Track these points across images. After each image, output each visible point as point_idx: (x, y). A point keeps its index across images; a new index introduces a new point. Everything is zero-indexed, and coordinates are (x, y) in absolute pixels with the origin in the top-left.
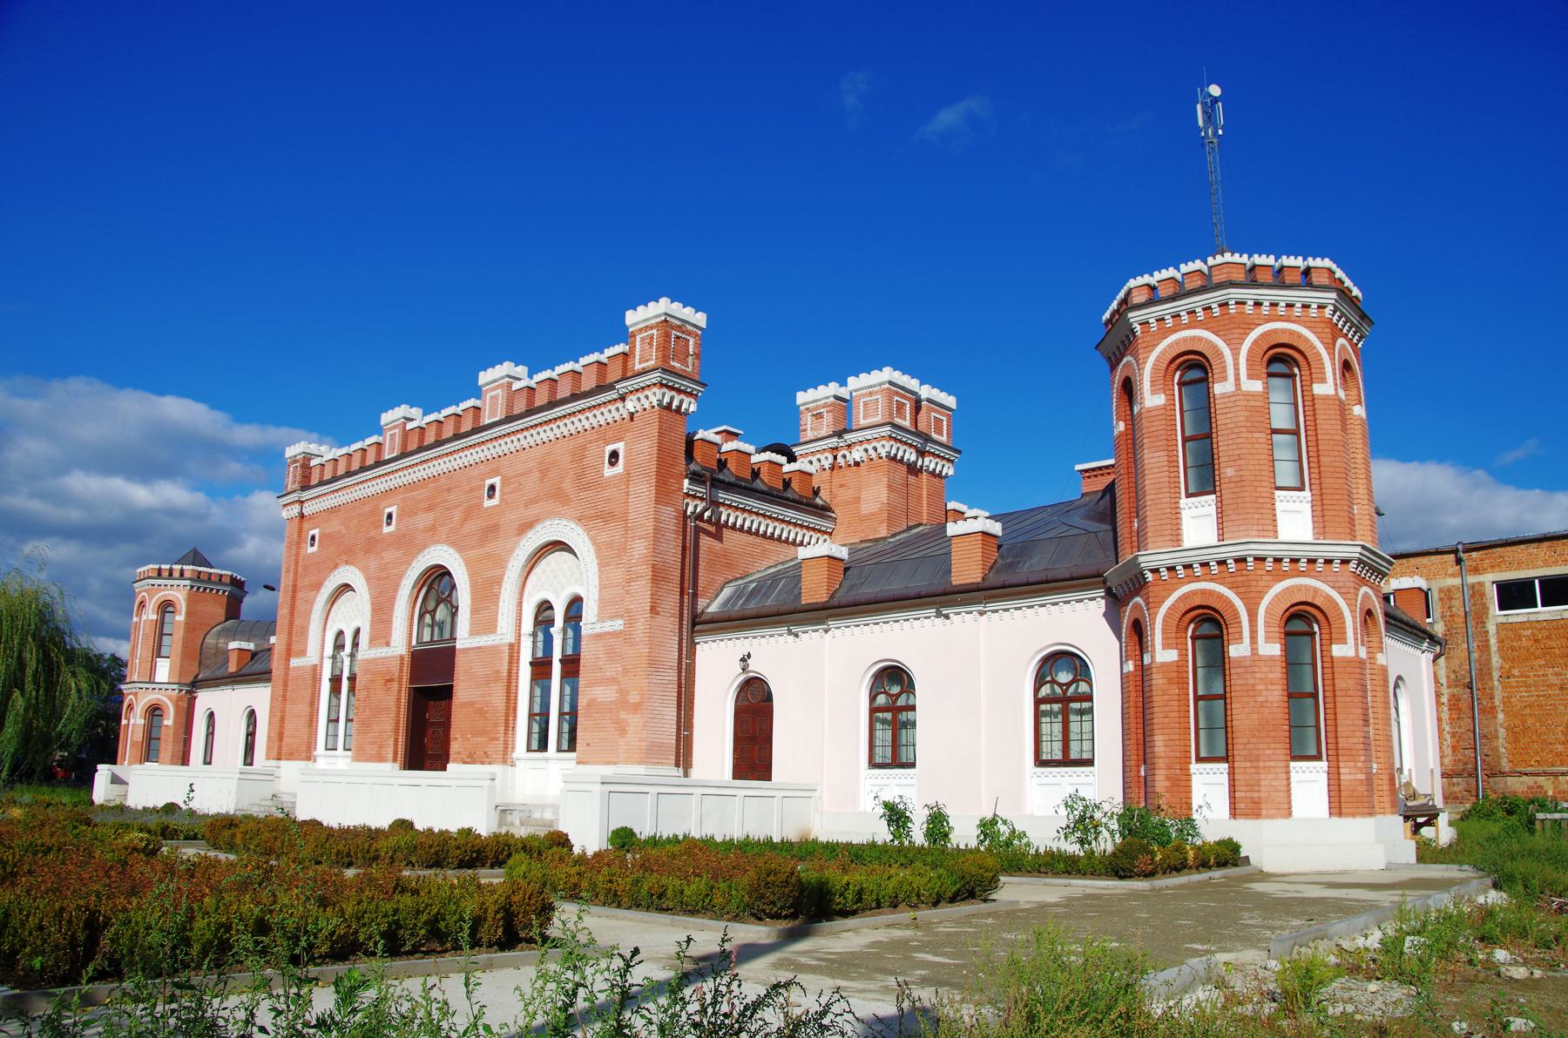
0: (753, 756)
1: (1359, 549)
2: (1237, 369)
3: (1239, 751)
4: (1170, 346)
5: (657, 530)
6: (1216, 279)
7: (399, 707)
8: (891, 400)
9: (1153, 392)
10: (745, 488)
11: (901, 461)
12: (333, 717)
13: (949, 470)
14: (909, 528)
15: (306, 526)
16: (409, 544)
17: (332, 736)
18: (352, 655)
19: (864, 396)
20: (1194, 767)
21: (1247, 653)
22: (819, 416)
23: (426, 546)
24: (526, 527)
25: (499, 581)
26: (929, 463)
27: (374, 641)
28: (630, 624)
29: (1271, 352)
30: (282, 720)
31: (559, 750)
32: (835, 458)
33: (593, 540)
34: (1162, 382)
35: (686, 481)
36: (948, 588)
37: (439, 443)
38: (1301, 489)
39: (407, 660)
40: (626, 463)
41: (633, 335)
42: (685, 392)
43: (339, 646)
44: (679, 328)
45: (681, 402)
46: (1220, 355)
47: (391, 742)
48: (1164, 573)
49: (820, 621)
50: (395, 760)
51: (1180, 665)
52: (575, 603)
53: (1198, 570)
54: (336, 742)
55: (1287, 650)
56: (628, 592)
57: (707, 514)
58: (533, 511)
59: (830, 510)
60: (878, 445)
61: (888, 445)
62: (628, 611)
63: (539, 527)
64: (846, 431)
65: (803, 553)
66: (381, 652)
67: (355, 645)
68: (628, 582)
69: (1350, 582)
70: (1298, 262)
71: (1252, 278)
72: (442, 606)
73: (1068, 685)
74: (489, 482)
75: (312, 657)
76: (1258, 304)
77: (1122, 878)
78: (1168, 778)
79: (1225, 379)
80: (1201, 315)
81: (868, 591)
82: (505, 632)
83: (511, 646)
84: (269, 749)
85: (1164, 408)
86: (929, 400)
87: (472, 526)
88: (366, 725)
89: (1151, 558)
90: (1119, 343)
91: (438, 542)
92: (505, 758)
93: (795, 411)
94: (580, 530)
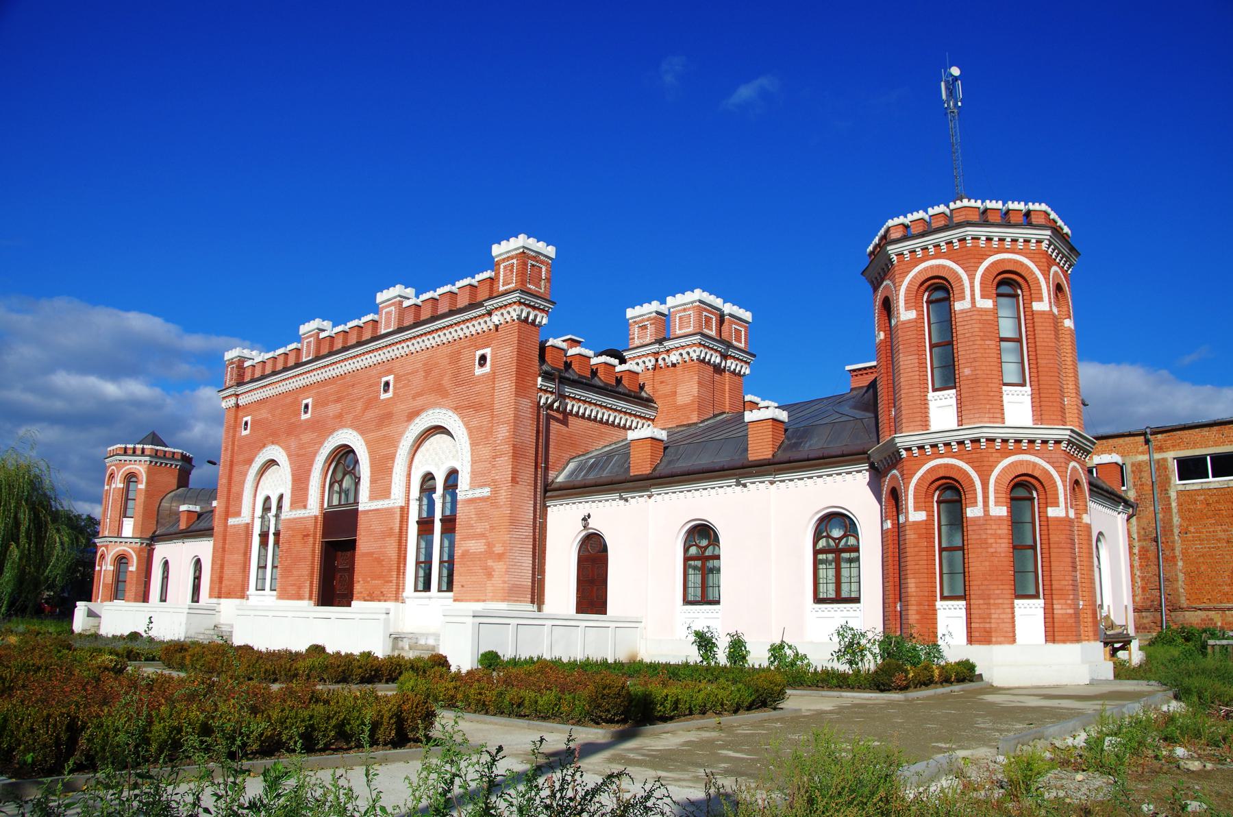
1: (1068, 432)
2: (972, 290)
3: (974, 591)
4: (920, 272)
5: (517, 417)
7: (313, 557)
8: (700, 315)
9: (907, 309)
11: (709, 363)
13: (746, 370)
15: (241, 414)
16: (322, 428)
18: (277, 516)
19: (679, 311)
21: (981, 514)
23: (334, 430)
24: (413, 415)
25: (392, 457)
26: (731, 364)
27: (294, 505)
28: (495, 491)
29: (1000, 277)
31: (440, 590)
32: (657, 360)
33: (466, 425)
35: (540, 379)
36: (746, 463)
38: (1023, 385)
39: (320, 519)
40: (492, 365)
41: (498, 264)
42: (538, 309)
43: (266, 509)
44: (534, 258)
45: (536, 316)
46: (959, 279)
48: (915, 451)
49: (645, 489)
50: (310, 598)
51: (928, 523)
52: (452, 475)
53: (942, 448)
54: (264, 584)
55: (1012, 511)
56: (494, 466)
57: (556, 405)
58: (419, 402)
59: (652, 401)
60: (691, 351)
61: (698, 350)
62: (494, 481)
63: (424, 415)
64: (665, 339)
65: (631, 435)
66: (300, 513)
67: (279, 507)
69: (1061, 458)
70: (1021, 206)
71: (984, 218)
72: (347, 477)
73: (840, 539)
74: (384, 379)
75: (245, 517)
76: (989, 239)
77: (882, 691)
78: (918, 612)
80: (944, 248)
81: (682, 465)
82: (397, 497)
83: (402, 508)
84: (211, 589)
85: (915, 321)
86: (730, 315)
87: (370, 414)
88: (287, 571)
89: (905, 439)
90: (880, 270)
92: (397, 597)
94: (456, 417)
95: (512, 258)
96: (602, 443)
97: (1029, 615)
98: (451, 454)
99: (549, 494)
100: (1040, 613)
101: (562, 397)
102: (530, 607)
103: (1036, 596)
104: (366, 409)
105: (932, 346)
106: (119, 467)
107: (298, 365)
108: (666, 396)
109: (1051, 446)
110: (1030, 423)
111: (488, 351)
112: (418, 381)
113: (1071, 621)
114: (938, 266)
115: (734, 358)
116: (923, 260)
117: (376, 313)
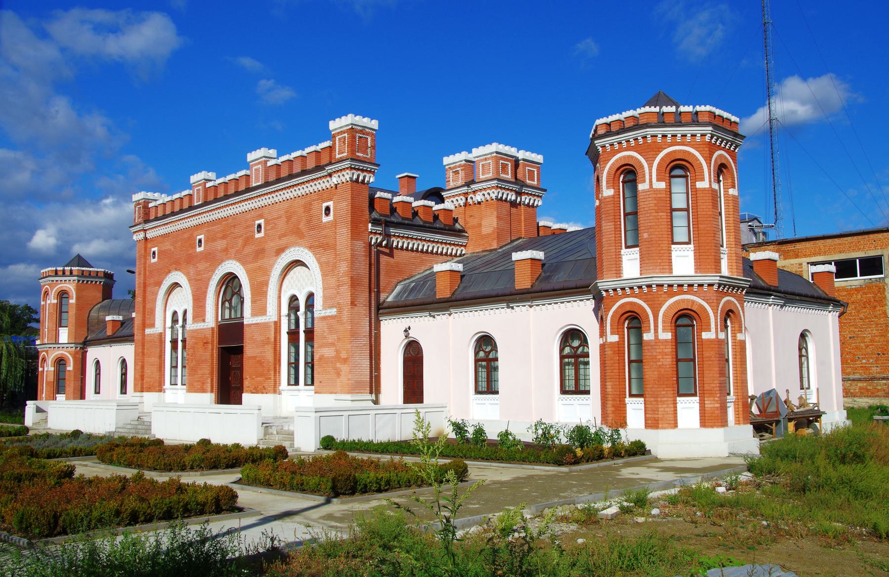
0: (413, 390)
1: (718, 278)
2: (651, 176)
3: (648, 392)
5: (353, 256)
6: (641, 122)
7: (212, 360)
8: (497, 163)
9: (608, 188)
10: (408, 225)
11: (506, 200)
12: (174, 365)
13: (540, 203)
14: (512, 241)
15: (149, 245)
16: (213, 260)
17: (174, 376)
18: (183, 327)
19: (482, 160)
20: (624, 251)
21: (653, 338)
22: (457, 172)
23: (222, 261)
24: (280, 251)
25: (266, 284)
26: (526, 199)
28: (340, 311)
29: (672, 164)
30: (143, 367)
31: (306, 384)
32: (467, 199)
33: (318, 260)
34: (613, 183)
35: (370, 225)
36: (513, 291)
37: (227, 197)
38: (689, 243)
40: (334, 215)
41: (334, 136)
42: (366, 171)
43: (175, 321)
44: (361, 132)
45: (364, 177)
46: (642, 167)
47: (209, 381)
48: (611, 292)
49: (446, 309)
50: (212, 391)
51: (620, 344)
52: (310, 296)
53: (628, 291)
54: (176, 380)
55: (676, 336)
57: (384, 243)
58: (284, 241)
59: (464, 231)
60: (491, 192)
61: (496, 192)
62: (339, 304)
63: (287, 251)
64: (473, 182)
65: (437, 268)
67: (185, 320)
68: (339, 286)
69: (713, 296)
70: (689, 109)
71: (662, 121)
72: (235, 296)
73: (578, 348)
74: (257, 222)
75: (158, 328)
76: (664, 136)
77: (559, 465)
78: (613, 406)
79: (644, 181)
80: (633, 143)
81: (473, 291)
83: (275, 323)
84: (135, 385)
85: (613, 197)
86: (524, 160)
87: (248, 250)
88: (193, 371)
90: (594, 156)
91: (228, 258)
92: (275, 390)
93: (443, 169)
95: (344, 132)
96: (423, 268)
97: (688, 409)
98: (308, 281)
99: (381, 311)
100: (697, 406)
101: (388, 236)
102: (369, 397)
103: (695, 395)
104: (245, 245)
105: (626, 215)
106: (52, 286)
107: (191, 208)
108: (474, 227)
109: (705, 288)
110: (692, 273)
111: (330, 204)
112: (282, 225)
113: (717, 412)
114: (629, 156)
115: (527, 194)
116: (619, 151)
117: (248, 169)
